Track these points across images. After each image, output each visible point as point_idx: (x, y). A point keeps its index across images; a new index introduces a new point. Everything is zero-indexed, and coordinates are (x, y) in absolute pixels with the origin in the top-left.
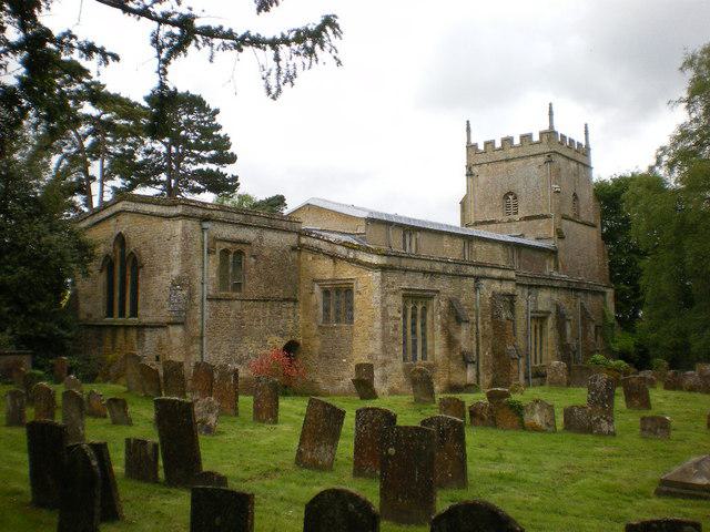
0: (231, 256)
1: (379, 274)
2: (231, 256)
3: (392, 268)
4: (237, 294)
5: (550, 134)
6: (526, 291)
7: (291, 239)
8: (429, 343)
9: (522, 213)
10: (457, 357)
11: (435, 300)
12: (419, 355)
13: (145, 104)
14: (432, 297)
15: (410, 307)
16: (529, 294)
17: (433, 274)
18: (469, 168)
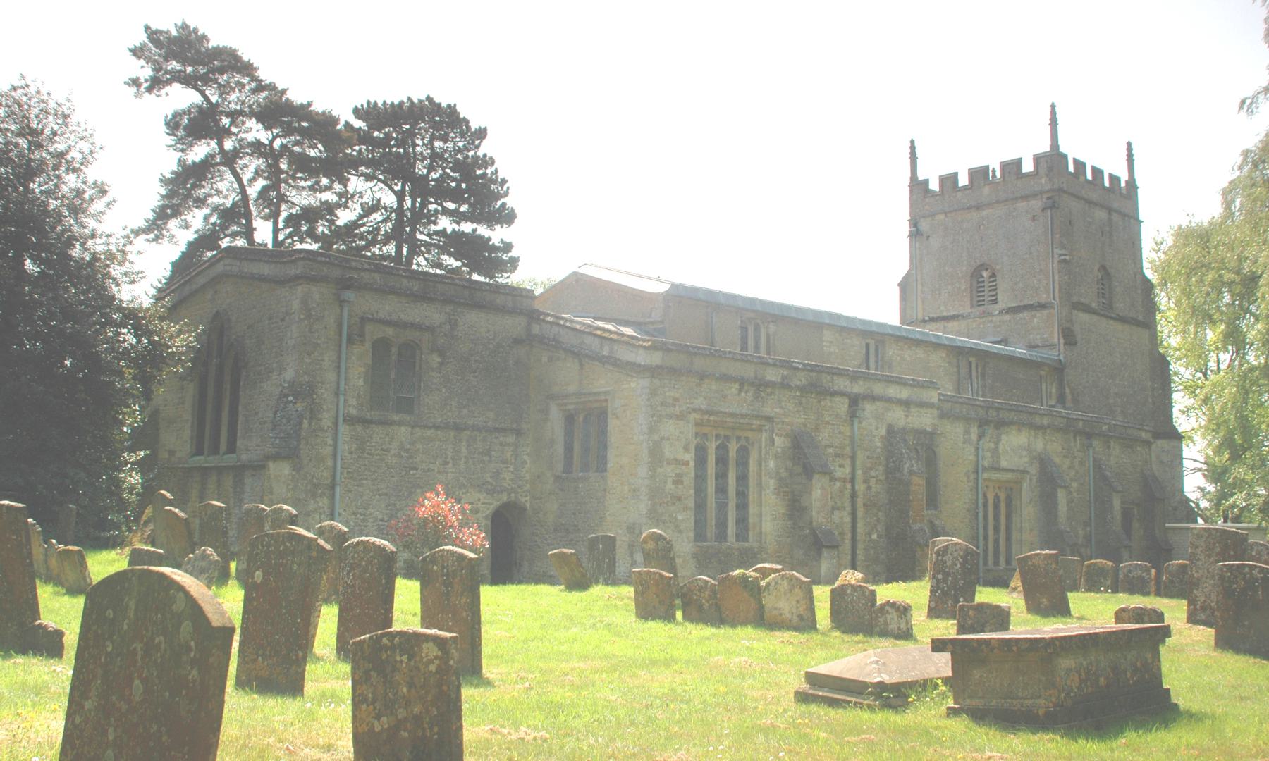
0: (394, 350)
2: (394, 350)
3: (673, 371)
5: (1052, 160)
8: (752, 510)
9: (1004, 301)
13: (359, 124)
16: (980, 437)
18: (914, 223)
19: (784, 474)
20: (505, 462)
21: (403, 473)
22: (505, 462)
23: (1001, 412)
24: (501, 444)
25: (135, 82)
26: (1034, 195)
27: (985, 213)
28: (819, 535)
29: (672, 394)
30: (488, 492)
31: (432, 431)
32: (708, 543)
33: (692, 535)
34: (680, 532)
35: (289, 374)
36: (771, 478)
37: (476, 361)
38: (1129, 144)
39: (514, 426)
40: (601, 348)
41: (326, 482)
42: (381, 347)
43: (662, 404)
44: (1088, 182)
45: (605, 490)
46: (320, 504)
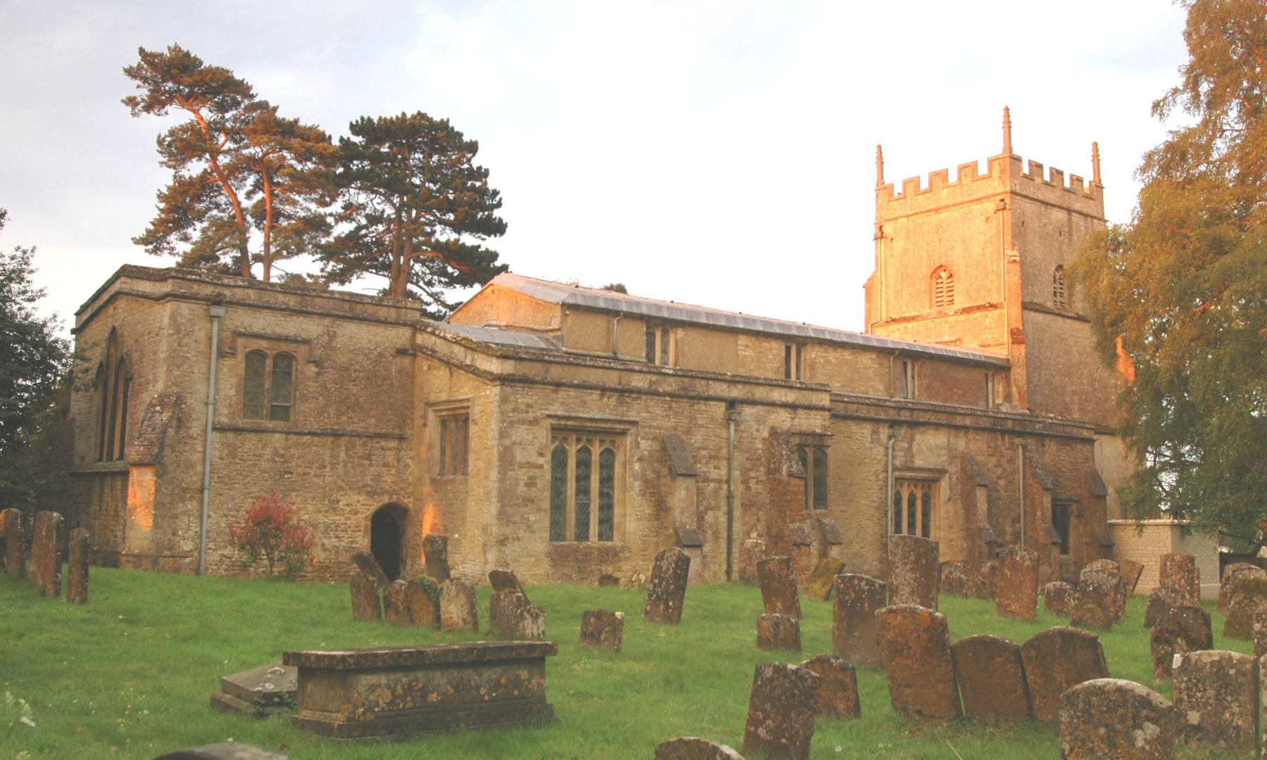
0: (269, 362)
1: (497, 390)
2: (269, 362)
4: (280, 424)
6: (884, 432)
7: (399, 336)
9: (960, 302)
10: (670, 536)
11: (629, 440)
12: (594, 528)
14: (623, 433)
15: (572, 449)
17: (624, 392)
19: (651, 475)
20: (385, 465)
21: (277, 477)
22: (385, 465)
23: (915, 412)
24: (382, 448)
25: (131, 102)
26: (988, 197)
27: (944, 215)
28: (681, 535)
29: (526, 401)
30: (368, 493)
31: (308, 437)
32: (566, 543)
33: (546, 535)
34: (533, 532)
35: (160, 386)
36: (636, 480)
37: (355, 371)
38: (1095, 145)
39: (397, 431)
40: (466, 357)
41: (196, 486)
42: (255, 358)
43: (514, 410)
44: (1046, 184)
45: (466, 492)
46: (189, 507)
